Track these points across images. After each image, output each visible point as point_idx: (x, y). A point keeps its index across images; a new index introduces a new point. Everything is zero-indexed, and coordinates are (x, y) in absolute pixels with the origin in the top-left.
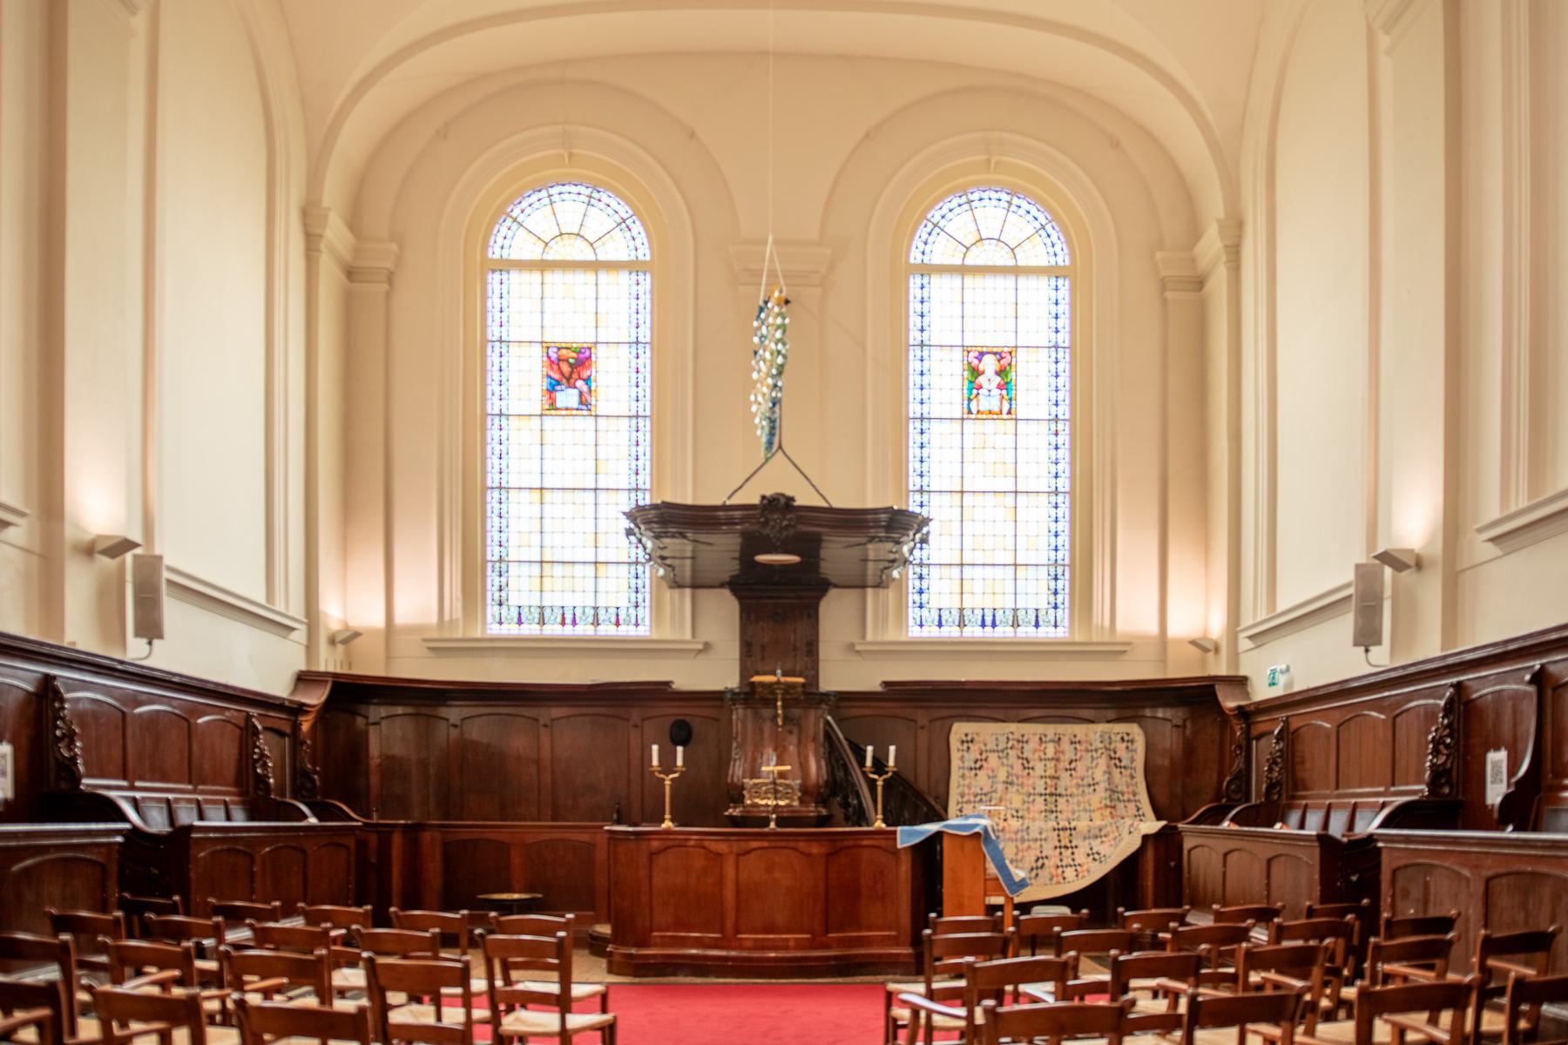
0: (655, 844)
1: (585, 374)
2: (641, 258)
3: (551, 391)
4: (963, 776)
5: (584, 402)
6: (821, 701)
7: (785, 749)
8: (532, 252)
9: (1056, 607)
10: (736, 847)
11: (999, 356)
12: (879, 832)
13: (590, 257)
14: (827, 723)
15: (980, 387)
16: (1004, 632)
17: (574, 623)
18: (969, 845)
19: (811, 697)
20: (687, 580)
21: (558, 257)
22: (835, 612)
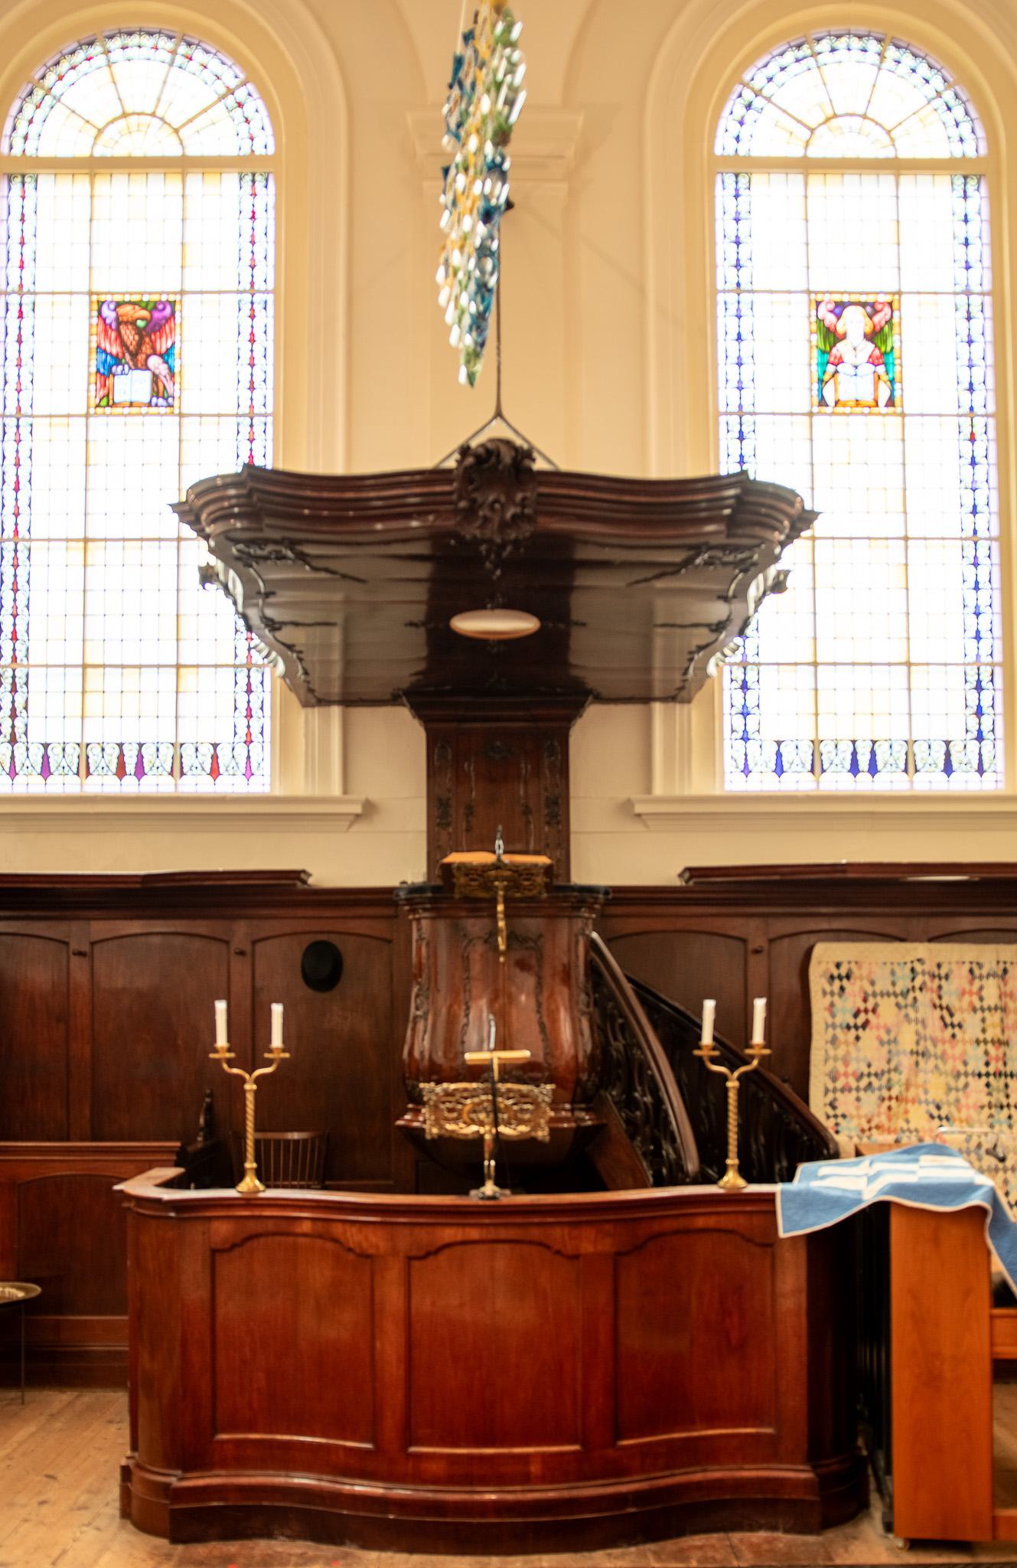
0: (222, 1230)
1: (163, 345)
2: (259, 151)
3: (105, 374)
4: (834, 1041)
5: (158, 390)
6: (580, 904)
7: (511, 999)
8: (79, 147)
9: (980, 738)
10: (405, 1239)
11: (872, 309)
12: (734, 1198)
13: (173, 150)
14: (592, 944)
15: (840, 361)
16: (890, 781)
17: (140, 772)
18: (953, 1235)
19: (560, 895)
20: (330, 686)
21: (120, 152)
22: (598, 743)
